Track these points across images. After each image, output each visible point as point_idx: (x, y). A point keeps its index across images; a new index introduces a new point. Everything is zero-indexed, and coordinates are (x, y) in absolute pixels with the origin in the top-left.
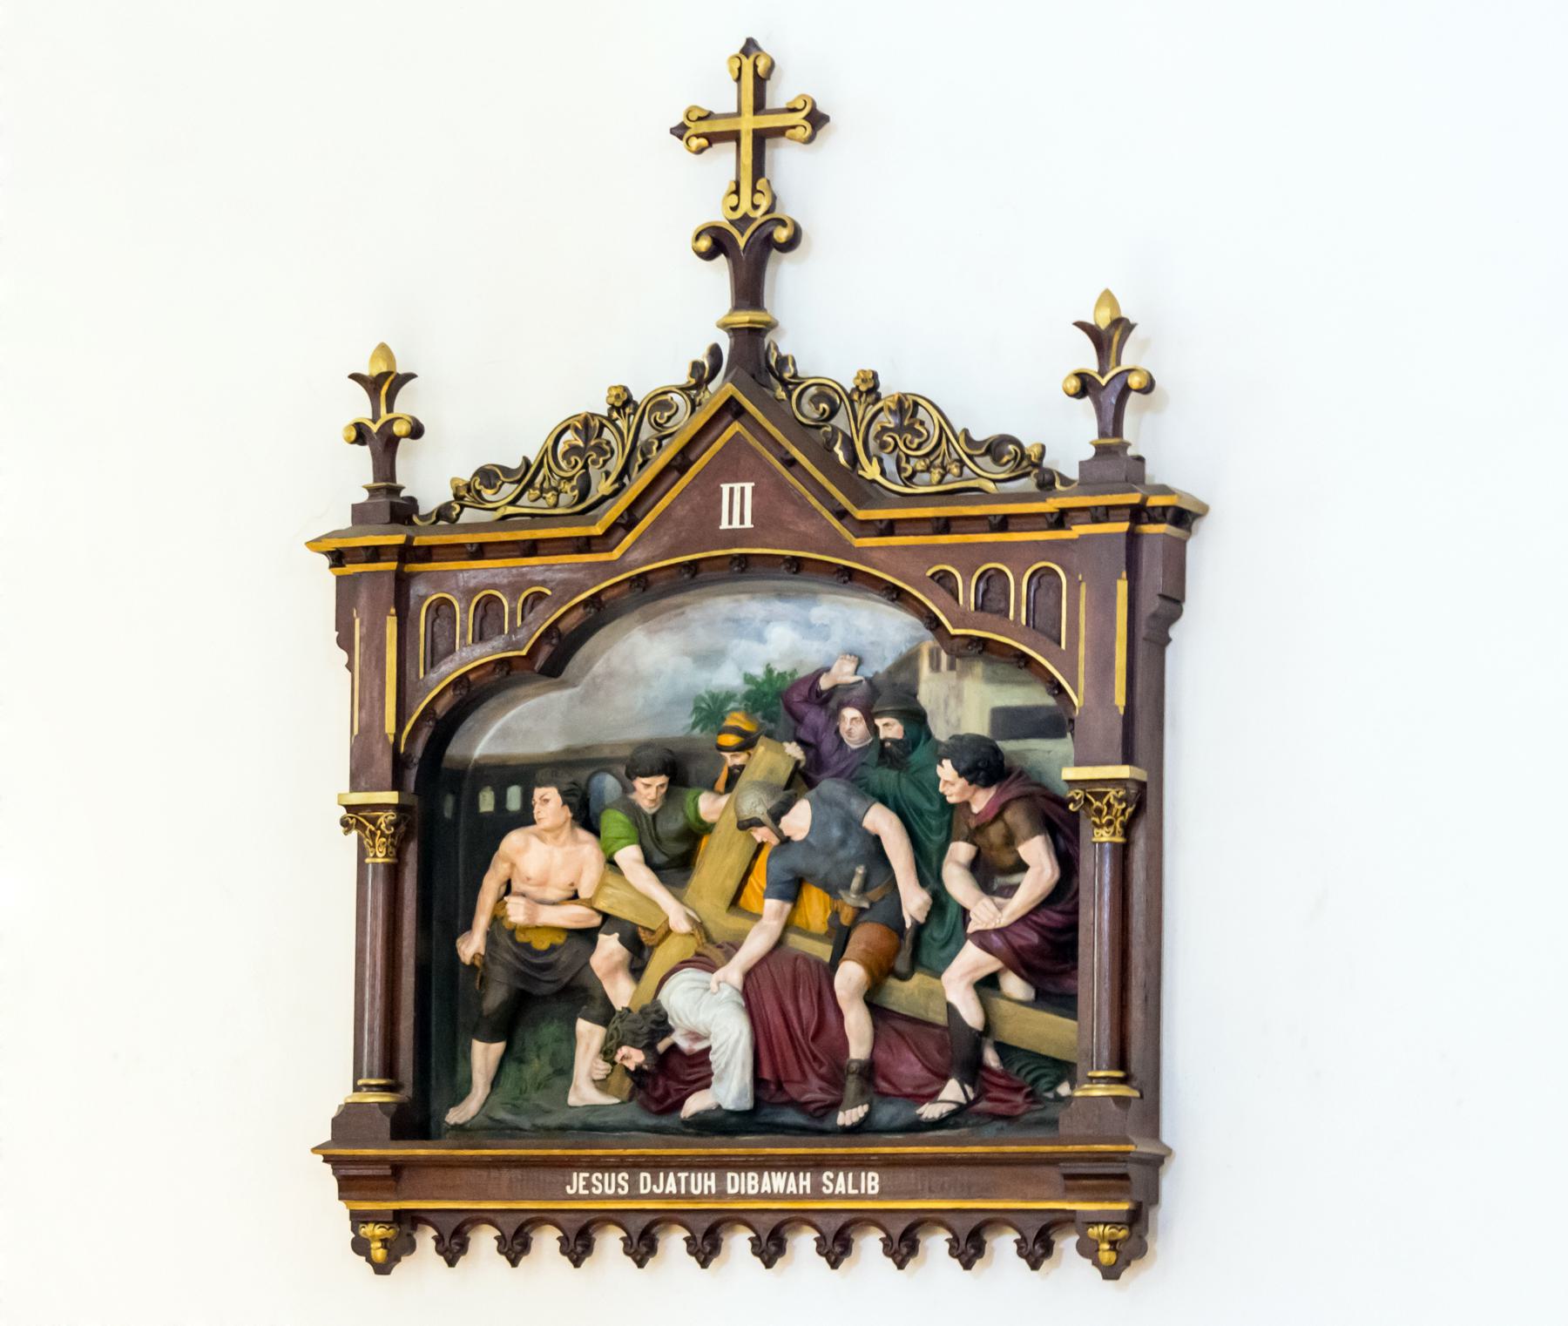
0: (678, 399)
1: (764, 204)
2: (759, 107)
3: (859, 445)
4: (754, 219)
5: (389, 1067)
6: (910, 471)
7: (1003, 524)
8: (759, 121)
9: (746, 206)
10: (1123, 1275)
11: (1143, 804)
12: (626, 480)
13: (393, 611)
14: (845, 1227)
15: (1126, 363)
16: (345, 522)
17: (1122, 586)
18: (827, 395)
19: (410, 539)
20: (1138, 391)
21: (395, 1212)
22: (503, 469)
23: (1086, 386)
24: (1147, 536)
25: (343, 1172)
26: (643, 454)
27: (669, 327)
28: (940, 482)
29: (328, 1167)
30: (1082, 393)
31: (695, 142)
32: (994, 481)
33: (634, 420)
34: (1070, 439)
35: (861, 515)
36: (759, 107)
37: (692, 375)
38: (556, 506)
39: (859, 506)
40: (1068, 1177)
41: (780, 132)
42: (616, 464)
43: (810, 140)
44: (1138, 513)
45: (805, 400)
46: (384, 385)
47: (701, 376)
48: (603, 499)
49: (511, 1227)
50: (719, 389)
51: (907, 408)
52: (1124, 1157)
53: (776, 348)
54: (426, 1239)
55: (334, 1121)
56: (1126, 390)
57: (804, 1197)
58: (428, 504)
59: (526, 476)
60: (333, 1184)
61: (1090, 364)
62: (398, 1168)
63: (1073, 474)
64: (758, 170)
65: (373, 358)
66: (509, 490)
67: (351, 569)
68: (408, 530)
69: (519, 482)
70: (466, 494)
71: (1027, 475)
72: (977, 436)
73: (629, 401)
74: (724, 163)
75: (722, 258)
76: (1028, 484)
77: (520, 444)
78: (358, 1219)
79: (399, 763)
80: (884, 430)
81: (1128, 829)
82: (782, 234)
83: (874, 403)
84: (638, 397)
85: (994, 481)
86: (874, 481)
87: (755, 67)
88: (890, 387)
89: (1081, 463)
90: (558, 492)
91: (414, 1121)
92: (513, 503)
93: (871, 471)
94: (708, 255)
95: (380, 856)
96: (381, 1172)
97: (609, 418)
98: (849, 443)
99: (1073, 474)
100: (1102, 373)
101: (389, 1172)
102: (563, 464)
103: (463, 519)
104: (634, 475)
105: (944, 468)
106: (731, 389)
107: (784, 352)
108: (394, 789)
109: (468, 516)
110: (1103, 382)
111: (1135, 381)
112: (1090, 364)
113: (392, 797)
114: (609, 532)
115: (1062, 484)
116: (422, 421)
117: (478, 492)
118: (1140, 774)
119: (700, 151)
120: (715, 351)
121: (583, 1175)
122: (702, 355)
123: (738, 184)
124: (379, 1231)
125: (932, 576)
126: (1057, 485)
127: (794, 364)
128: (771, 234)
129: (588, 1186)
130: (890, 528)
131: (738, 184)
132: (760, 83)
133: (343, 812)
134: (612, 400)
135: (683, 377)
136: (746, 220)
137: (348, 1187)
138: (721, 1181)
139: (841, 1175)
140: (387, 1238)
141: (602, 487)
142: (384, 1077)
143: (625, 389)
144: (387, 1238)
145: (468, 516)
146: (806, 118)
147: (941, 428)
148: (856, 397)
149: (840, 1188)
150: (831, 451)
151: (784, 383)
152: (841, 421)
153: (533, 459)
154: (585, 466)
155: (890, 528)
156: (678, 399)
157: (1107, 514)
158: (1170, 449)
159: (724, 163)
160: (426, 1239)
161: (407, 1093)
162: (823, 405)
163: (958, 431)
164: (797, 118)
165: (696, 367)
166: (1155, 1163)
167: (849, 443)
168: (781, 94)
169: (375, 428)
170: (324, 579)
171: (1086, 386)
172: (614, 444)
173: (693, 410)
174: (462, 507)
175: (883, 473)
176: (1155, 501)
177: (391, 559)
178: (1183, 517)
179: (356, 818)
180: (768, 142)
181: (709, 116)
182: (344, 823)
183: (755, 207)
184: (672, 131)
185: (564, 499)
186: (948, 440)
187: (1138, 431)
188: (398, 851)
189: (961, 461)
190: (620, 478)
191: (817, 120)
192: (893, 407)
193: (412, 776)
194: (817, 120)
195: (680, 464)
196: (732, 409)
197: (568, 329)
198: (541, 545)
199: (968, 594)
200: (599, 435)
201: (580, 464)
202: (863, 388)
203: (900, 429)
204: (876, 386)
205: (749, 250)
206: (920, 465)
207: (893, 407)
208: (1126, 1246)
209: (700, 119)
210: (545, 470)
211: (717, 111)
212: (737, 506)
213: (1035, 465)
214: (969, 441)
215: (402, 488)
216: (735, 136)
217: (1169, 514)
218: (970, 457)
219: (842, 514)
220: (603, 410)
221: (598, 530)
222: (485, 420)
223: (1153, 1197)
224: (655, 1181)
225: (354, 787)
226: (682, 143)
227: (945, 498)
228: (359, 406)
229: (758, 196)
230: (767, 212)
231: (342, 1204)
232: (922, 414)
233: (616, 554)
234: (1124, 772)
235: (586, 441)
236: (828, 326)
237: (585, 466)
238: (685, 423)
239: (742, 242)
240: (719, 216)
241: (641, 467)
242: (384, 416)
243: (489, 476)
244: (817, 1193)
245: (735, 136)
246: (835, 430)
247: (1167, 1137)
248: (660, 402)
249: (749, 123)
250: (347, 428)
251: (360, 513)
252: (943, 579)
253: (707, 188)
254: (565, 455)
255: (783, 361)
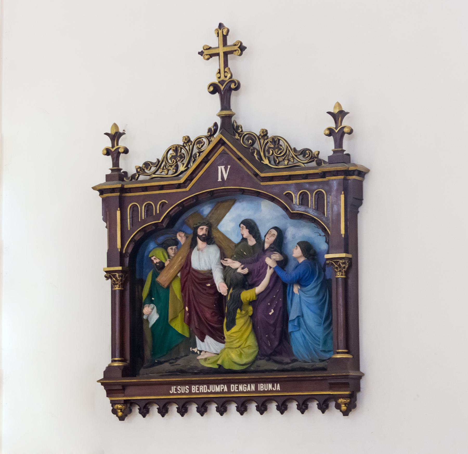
0: (205, 140)
1: (229, 76)
2: (225, 44)
3: (262, 154)
4: (225, 81)
5: (122, 354)
6: (278, 161)
7: (162, 187)
8: (226, 49)
9: (223, 78)
10: (350, 414)
11: (352, 266)
12: (189, 166)
13: (119, 209)
14: (146, 404)
15: (343, 125)
16: (103, 180)
17: (342, 197)
18: (252, 137)
19: (123, 185)
20: (123, 153)
21: (125, 400)
22: (151, 163)
23: (331, 132)
24: (350, 179)
25: (108, 388)
26: (194, 158)
27: (203, 116)
28: (287, 165)
29: (103, 387)
30: (329, 135)
31: (207, 57)
32: (303, 163)
33: (191, 146)
34: (326, 148)
35: (262, 175)
36: (225, 44)
37: (208, 132)
38: (167, 174)
39: (261, 172)
40: (331, 384)
41: (231, 52)
42: (185, 162)
43: (241, 55)
44: (347, 173)
45: (245, 138)
46: (115, 136)
47: (212, 132)
48: (182, 172)
49: (162, 404)
50: (217, 136)
51: (276, 141)
52: (346, 377)
53: (236, 122)
54: (136, 409)
55: (104, 372)
56: (343, 133)
57: (253, 392)
58: (130, 175)
59: (158, 164)
60: (105, 392)
61: (333, 125)
62: (124, 387)
63: (327, 160)
64: (226, 65)
65: (335, 107)
66: (153, 169)
67: (105, 195)
68: (123, 183)
69: (156, 166)
70: (141, 170)
71: (313, 161)
72: (299, 149)
73: (266, 135)
74: (215, 64)
75: (217, 94)
76: (314, 164)
77: (156, 155)
78: (113, 403)
79: (122, 256)
80: (270, 148)
81: (347, 273)
82: (233, 86)
83: (267, 139)
84: (192, 139)
85: (303, 163)
86: (267, 165)
87: (223, 32)
88: (270, 134)
89: (329, 157)
90: (168, 170)
91: (129, 371)
92: (154, 173)
93: (266, 162)
94: (213, 93)
95: (117, 288)
96: (119, 388)
97: (183, 146)
98: (259, 153)
99: (327, 160)
100: (336, 128)
101: (121, 388)
102: (170, 161)
103: (139, 179)
104: (191, 164)
105: (167, 169)
106: (221, 136)
107: (238, 124)
108: (120, 266)
109: (142, 178)
110: (337, 131)
111: (346, 130)
112: (333, 125)
113: (120, 268)
114: (185, 182)
115: (324, 163)
116: (128, 148)
117: (144, 170)
118: (350, 256)
119: (208, 59)
120: (216, 124)
121: (175, 387)
122: (211, 125)
123: (220, 70)
124: (119, 406)
125: (285, 194)
126: (323, 163)
127: (241, 128)
128: (230, 86)
129: (176, 390)
130: (272, 179)
131: (220, 70)
132: (225, 38)
133: (105, 273)
134: (184, 140)
135: (205, 133)
136: (222, 82)
137: (110, 393)
138: (229, 388)
139: (249, 385)
140: (123, 410)
141: (181, 168)
142: (120, 357)
143: (188, 137)
144: (123, 410)
145: (142, 178)
146: (239, 47)
147: (287, 147)
148: (185, 145)
149: (249, 389)
150: (253, 155)
151: (239, 134)
152: (257, 146)
153: (160, 159)
154: (177, 162)
155: (272, 179)
156: (205, 140)
157: (338, 174)
158: (360, 151)
159: (215, 64)
160: (136, 409)
161: (128, 362)
162: (250, 141)
163: (292, 148)
164: (236, 48)
165: (210, 130)
166: (359, 378)
167: (259, 153)
168: (230, 42)
169: (113, 150)
170: (98, 200)
171: (331, 132)
172: (185, 155)
173: (209, 143)
174: (139, 175)
175: (270, 162)
176: (351, 168)
177: (118, 194)
178: (362, 173)
179: (109, 275)
180: (229, 56)
181: (210, 48)
182: (106, 277)
183: (226, 77)
184: (199, 53)
185: (171, 172)
186: (289, 151)
187: (346, 145)
188: (123, 285)
189: (293, 157)
190: (187, 166)
191: (242, 48)
192: (271, 140)
193: (127, 260)
194: (242, 48)
195: (205, 161)
196: (221, 142)
197: (169, 118)
198: (148, 188)
199: (296, 200)
200: (181, 152)
201: (175, 162)
202: (262, 134)
203: (274, 149)
204: (267, 134)
205: (225, 89)
206: (281, 159)
207: (174, 149)
208: (350, 407)
209: (207, 49)
210: (164, 163)
211: (213, 47)
212: (223, 172)
213: (316, 158)
214: (295, 150)
215: (121, 169)
216: (218, 54)
217: (356, 173)
218: (296, 156)
219: (256, 175)
220: (181, 143)
221: (182, 181)
222: (146, 148)
223: (358, 388)
224: (208, 388)
225: (108, 266)
226: (202, 57)
227: (288, 169)
228: (108, 143)
229: (226, 73)
230: (229, 79)
231: (108, 398)
232: (281, 143)
233: (188, 189)
234: (343, 255)
235: (275, 145)
236: (253, 115)
237: (177, 162)
238: (207, 148)
239: (222, 88)
240: (215, 80)
241: (193, 162)
242: (116, 147)
243: (147, 165)
244: (256, 391)
245: (218, 54)
246: (254, 148)
247: (362, 370)
248: (199, 141)
249: (221, 51)
250: (103, 151)
251: (108, 178)
252: (289, 195)
253: (210, 71)
254: (171, 159)
255: (238, 127)
